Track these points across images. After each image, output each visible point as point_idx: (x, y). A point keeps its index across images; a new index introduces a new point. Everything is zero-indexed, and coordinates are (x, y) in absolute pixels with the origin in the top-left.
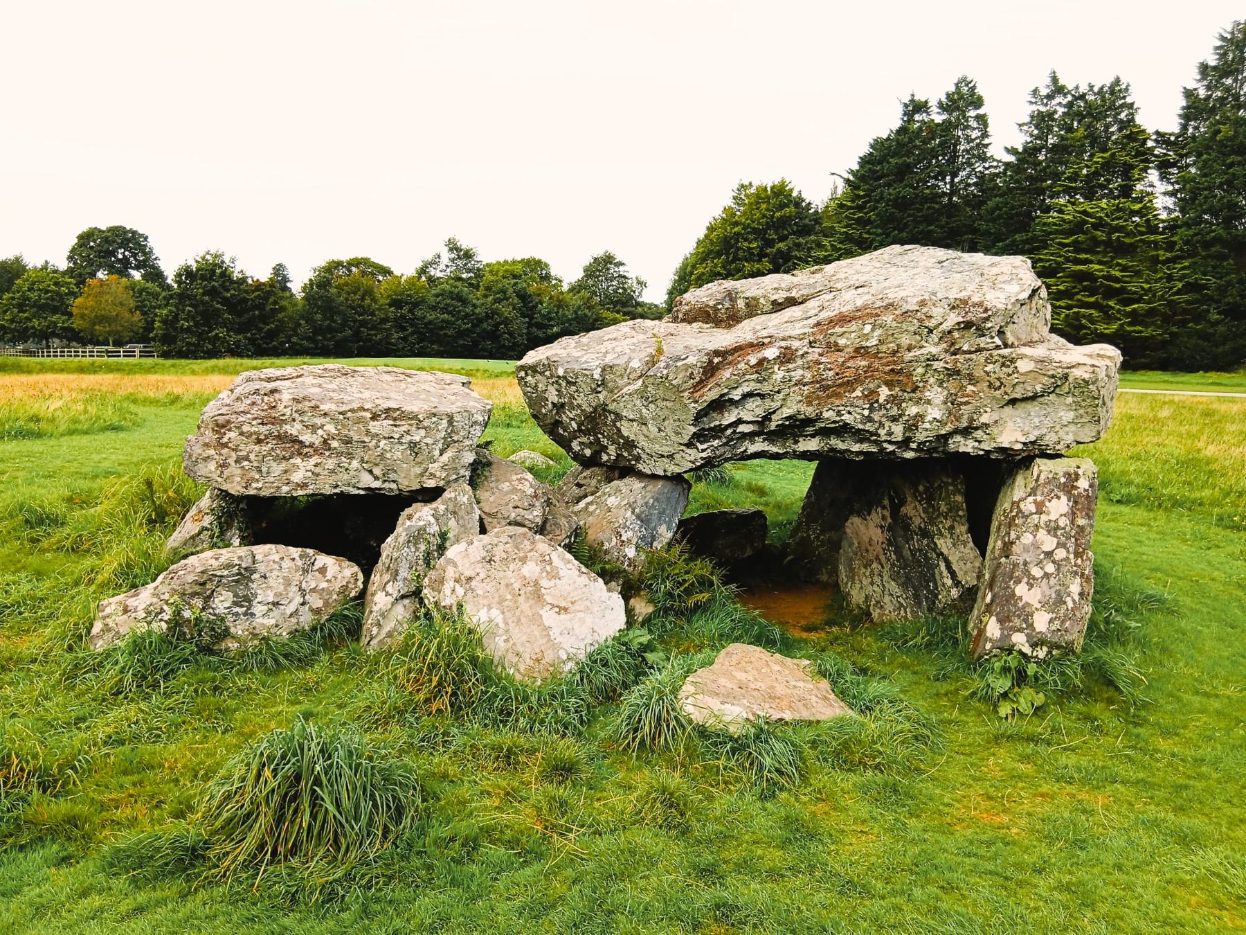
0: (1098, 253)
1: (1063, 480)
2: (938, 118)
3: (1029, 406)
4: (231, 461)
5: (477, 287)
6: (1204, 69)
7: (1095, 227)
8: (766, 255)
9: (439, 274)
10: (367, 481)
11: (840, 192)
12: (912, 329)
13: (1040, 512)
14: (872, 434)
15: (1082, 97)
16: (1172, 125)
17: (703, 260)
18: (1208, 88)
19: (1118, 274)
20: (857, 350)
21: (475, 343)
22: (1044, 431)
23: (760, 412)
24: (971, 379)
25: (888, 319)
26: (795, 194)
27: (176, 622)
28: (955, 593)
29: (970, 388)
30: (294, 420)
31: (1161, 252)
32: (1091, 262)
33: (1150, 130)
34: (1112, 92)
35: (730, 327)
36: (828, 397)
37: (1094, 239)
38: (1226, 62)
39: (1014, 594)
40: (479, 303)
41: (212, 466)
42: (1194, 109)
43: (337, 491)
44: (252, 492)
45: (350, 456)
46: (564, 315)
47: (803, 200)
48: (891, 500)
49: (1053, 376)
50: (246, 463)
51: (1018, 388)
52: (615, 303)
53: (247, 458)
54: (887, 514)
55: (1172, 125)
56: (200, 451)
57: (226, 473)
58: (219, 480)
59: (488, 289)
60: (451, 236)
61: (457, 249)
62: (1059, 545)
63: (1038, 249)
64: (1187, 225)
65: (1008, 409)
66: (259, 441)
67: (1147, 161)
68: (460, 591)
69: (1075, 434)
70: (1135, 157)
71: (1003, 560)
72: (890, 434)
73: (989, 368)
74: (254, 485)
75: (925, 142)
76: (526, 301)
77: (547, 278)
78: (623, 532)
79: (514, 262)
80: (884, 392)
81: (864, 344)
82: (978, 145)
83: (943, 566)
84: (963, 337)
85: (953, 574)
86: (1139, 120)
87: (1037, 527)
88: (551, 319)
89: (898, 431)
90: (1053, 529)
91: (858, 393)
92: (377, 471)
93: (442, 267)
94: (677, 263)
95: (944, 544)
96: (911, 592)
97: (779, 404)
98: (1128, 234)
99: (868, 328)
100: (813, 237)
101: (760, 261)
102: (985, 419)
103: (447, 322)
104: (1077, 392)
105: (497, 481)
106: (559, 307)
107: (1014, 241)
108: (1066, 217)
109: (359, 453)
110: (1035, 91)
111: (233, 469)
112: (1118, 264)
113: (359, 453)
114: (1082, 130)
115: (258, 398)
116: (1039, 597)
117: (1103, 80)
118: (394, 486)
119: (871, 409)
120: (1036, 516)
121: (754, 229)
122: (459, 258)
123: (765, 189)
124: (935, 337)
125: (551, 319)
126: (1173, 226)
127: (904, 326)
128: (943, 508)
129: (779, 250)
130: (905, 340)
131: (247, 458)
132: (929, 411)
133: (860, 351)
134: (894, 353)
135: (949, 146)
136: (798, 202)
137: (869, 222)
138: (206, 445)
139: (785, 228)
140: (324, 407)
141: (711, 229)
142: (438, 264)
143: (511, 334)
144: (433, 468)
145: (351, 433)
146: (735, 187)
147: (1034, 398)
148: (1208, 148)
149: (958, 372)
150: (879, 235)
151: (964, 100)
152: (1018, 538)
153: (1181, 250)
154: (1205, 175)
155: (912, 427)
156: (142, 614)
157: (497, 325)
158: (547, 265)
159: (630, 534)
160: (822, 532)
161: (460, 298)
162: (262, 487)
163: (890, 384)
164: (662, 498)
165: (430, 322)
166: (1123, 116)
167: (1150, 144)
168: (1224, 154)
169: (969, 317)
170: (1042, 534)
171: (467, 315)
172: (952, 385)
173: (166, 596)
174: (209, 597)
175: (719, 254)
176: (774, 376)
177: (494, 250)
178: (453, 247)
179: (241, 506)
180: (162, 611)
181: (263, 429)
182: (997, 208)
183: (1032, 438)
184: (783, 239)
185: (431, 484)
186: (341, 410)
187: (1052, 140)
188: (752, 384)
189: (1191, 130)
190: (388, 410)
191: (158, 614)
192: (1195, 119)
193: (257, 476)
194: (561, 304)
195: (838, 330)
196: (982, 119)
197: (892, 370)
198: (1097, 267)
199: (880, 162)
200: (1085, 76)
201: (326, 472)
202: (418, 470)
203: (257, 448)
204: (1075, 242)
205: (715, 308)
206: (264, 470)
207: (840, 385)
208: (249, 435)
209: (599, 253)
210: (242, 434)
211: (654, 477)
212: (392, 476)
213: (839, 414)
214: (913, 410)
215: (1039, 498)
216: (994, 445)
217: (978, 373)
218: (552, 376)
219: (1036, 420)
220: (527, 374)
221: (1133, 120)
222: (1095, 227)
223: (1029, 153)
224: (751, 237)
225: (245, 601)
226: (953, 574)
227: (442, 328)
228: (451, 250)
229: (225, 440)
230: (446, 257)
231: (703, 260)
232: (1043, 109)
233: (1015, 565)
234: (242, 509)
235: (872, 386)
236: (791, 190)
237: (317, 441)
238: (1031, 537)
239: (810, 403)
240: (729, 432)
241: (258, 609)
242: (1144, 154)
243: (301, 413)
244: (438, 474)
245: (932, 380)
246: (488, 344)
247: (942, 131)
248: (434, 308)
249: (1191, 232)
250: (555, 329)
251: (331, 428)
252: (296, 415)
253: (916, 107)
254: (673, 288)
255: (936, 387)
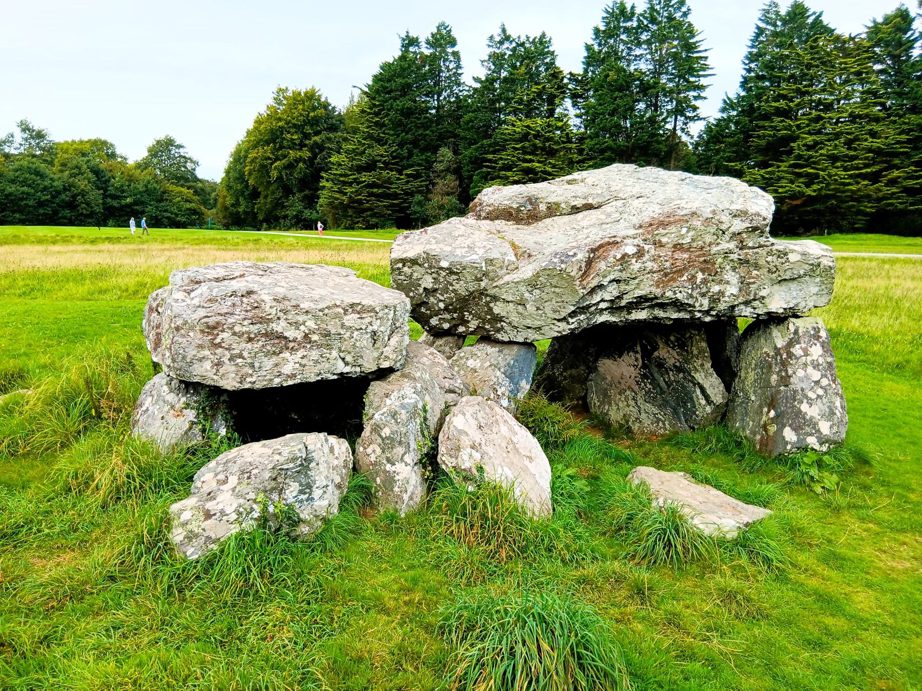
0: (537, 155)
1: (812, 332)
2: (427, 52)
3: (793, 285)
4: (225, 359)
5: (51, 163)
6: (597, 31)
7: (536, 136)
8: (305, 145)
9: (13, 152)
10: (341, 368)
11: (356, 100)
12: (712, 231)
13: (806, 355)
14: (690, 306)
15: (523, 44)
16: (579, 69)
17: (255, 147)
18: (600, 45)
19: (550, 170)
20: (675, 246)
21: (56, 212)
22: (800, 300)
23: (616, 293)
24: (757, 266)
25: (697, 223)
26: (323, 99)
27: (263, 521)
28: (708, 409)
29: (756, 272)
30: (279, 318)
31: (575, 156)
32: (532, 161)
33: (566, 72)
34: (541, 43)
35: (529, 224)
36: (669, 281)
37: (534, 145)
38: (610, 29)
39: (800, 411)
40: (56, 177)
41: (207, 365)
42: (592, 59)
43: (319, 378)
44: (247, 386)
45: (329, 347)
46: (136, 188)
47: (330, 105)
48: (642, 346)
49: (812, 265)
50: (240, 360)
51: (787, 273)
52: (179, 179)
53: (240, 356)
54: (639, 356)
55: (579, 69)
56: (194, 353)
57: (221, 370)
58: (215, 377)
59: (64, 165)
60: (23, 118)
61: (29, 130)
62: (822, 376)
63: (498, 151)
64: (591, 138)
65: (776, 287)
66: (250, 340)
67: (564, 92)
68: (477, 456)
69: (815, 301)
70: (557, 89)
71: (782, 388)
72: (701, 305)
73: (769, 259)
74: (248, 380)
75: (419, 68)
76: (100, 178)
77: (113, 156)
78: (498, 388)
79: (81, 142)
80: (700, 276)
81: (680, 242)
82: (454, 73)
83: (698, 391)
84: (749, 237)
85: (707, 397)
86: (558, 64)
87: (805, 365)
88: (123, 191)
89: (706, 303)
90: (816, 366)
91: (685, 278)
92: (349, 358)
93: (16, 145)
94: (232, 148)
95: (699, 377)
96: (669, 410)
97: (633, 287)
98: (557, 143)
99: (684, 230)
100: (339, 134)
101: (301, 149)
102: (763, 293)
103: (28, 194)
104: (823, 274)
105: (416, 357)
106: (130, 181)
107: (482, 145)
108: (518, 130)
109: (337, 344)
110: (491, 38)
111: (228, 367)
112: (550, 163)
113: (337, 344)
114: (523, 68)
115: (237, 300)
116: (818, 411)
117: (535, 34)
118: (358, 369)
119: (692, 289)
120: (804, 358)
121: (294, 124)
122: (32, 137)
123: (300, 94)
124: (727, 236)
125: (123, 191)
126: (581, 139)
127: (708, 229)
128: (695, 352)
129: (316, 143)
130: (708, 239)
131: (240, 356)
132: (728, 288)
133: (678, 247)
134: (702, 248)
135: (435, 73)
136: (326, 106)
137: (383, 125)
138: (201, 347)
139: (317, 125)
140: (305, 305)
141: (259, 122)
142: (12, 142)
143: (88, 204)
144: (388, 351)
145: (329, 327)
146: (275, 90)
147: (794, 279)
148: (602, 86)
149: (747, 262)
150: (392, 135)
151: (443, 40)
152: (794, 373)
153: (588, 154)
154: (600, 105)
155: (715, 300)
156: (234, 516)
157: (74, 196)
158: (112, 145)
159: (503, 389)
160: (565, 370)
161: (37, 173)
162: (258, 381)
163: (703, 271)
164: (521, 359)
165: (10, 194)
166: (547, 60)
167: (566, 81)
168: (611, 91)
169: (755, 224)
170: (810, 369)
171: (45, 188)
172: (742, 271)
173: (252, 496)
174: (282, 490)
175: (267, 143)
176: (632, 267)
177: (64, 130)
178: (25, 128)
179: (222, 398)
180: (252, 510)
181: (254, 329)
182: (471, 121)
183: (791, 305)
184: (317, 133)
185: (385, 365)
186: (320, 307)
187: (504, 74)
188: (616, 273)
189: (590, 73)
190: (352, 305)
191: (248, 513)
192: (593, 66)
193: (250, 372)
194: (131, 179)
195: (661, 231)
196: (456, 54)
197: (705, 261)
198: (537, 165)
199: (389, 81)
200: (524, 29)
201: (311, 363)
202: (376, 354)
203: (249, 345)
204: (523, 147)
205: (518, 210)
206: (257, 365)
207: (675, 273)
208: (240, 335)
209: (161, 136)
210: (234, 334)
211: (511, 343)
212: (360, 361)
213: (675, 293)
214: (716, 288)
215: (803, 346)
216: (766, 310)
217: (762, 262)
218: (430, 267)
219: (794, 293)
220: (404, 266)
221: (553, 63)
222: (536, 136)
223: (490, 81)
224: (293, 130)
225: (306, 488)
226: (707, 397)
227: (22, 199)
228: (24, 130)
229: (218, 341)
230: (19, 137)
231: (255, 147)
232: (497, 51)
233: (795, 391)
234: (224, 401)
235: (693, 272)
236: (319, 96)
237: (299, 335)
238: (803, 372)
239: (658, 287)
240: (593, 308)
241: (317, 493)
242: (563, 88)
243: (286, 312)
244: (391, 356)
245: (728, 267)
246: (67, 213)
247: (431, 61)
248: (13, 181)
249: (593, 143)
250: (128, 200)
251: (311, 324)
252: (281, 314)
253: (410, 42)
254: (230, 168)
255: (730, 272)
